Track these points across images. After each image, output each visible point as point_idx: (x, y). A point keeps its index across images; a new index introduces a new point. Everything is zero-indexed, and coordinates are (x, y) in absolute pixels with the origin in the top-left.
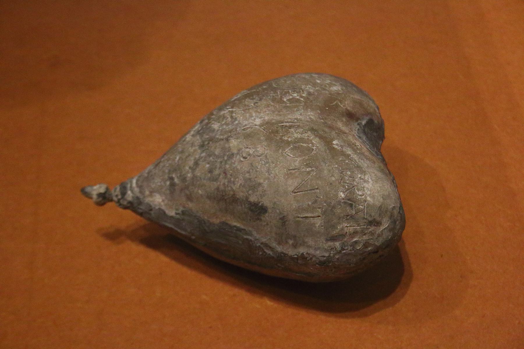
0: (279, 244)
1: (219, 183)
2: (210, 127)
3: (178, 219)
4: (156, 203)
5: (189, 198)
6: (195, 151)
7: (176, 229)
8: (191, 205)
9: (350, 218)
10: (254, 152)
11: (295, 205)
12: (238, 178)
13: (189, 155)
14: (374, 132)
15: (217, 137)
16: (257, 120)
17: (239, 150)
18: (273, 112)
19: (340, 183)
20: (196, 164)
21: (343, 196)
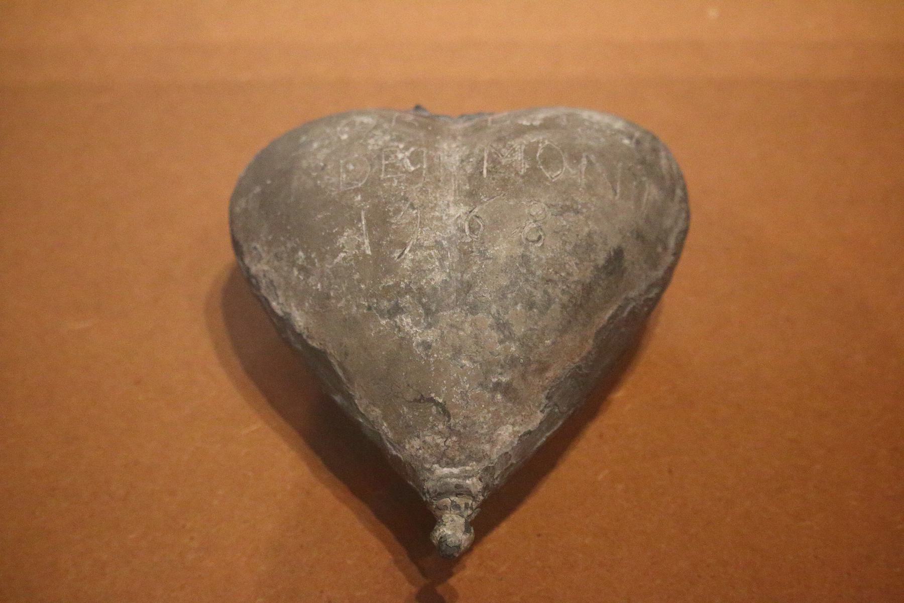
1: (557, 300)
5: (543, 368)
6: (473, 324)
8: (550, 374)
13: (476, 337)
20: (501, 326)
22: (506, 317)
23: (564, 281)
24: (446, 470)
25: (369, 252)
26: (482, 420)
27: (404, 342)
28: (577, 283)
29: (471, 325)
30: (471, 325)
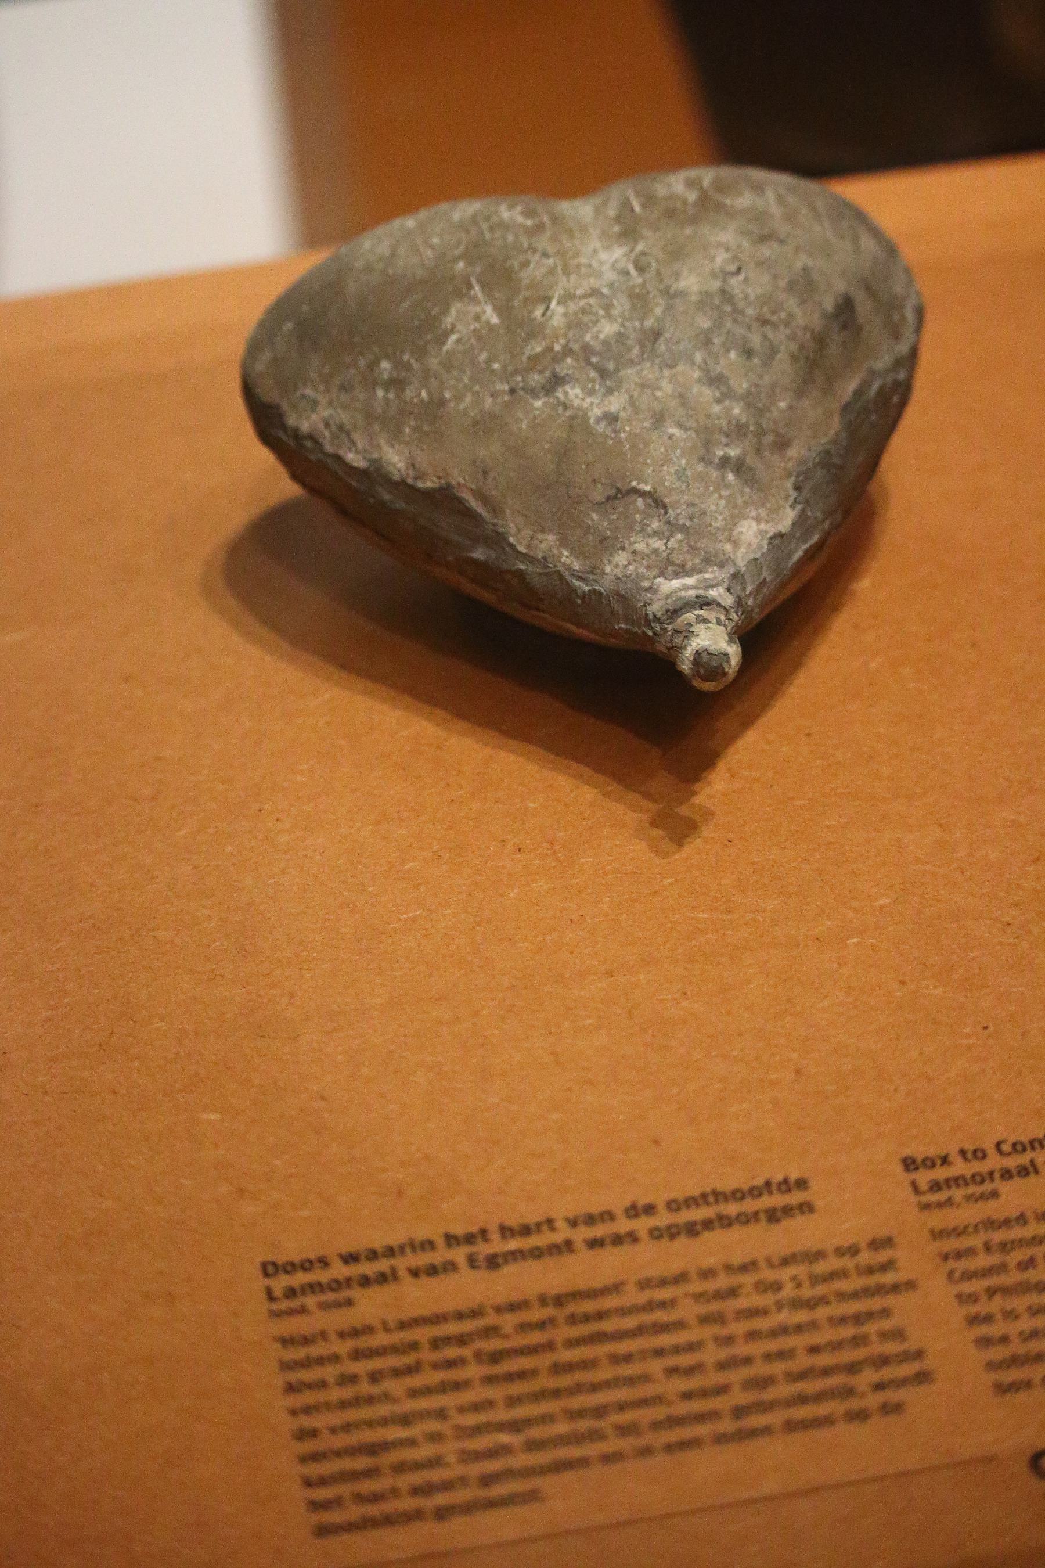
4: (755, 541)
5: (782, 445)
6: (673, 379)
8: (792, 452)
13: (681, 396)
20: (715, 380)
22: (718, 369)
24: (676, 583)
25: (495, 320)
26: (713, 508)
27: (577, 422)
28: (805, 328)
29: (670, 382)
30: (670, 382)
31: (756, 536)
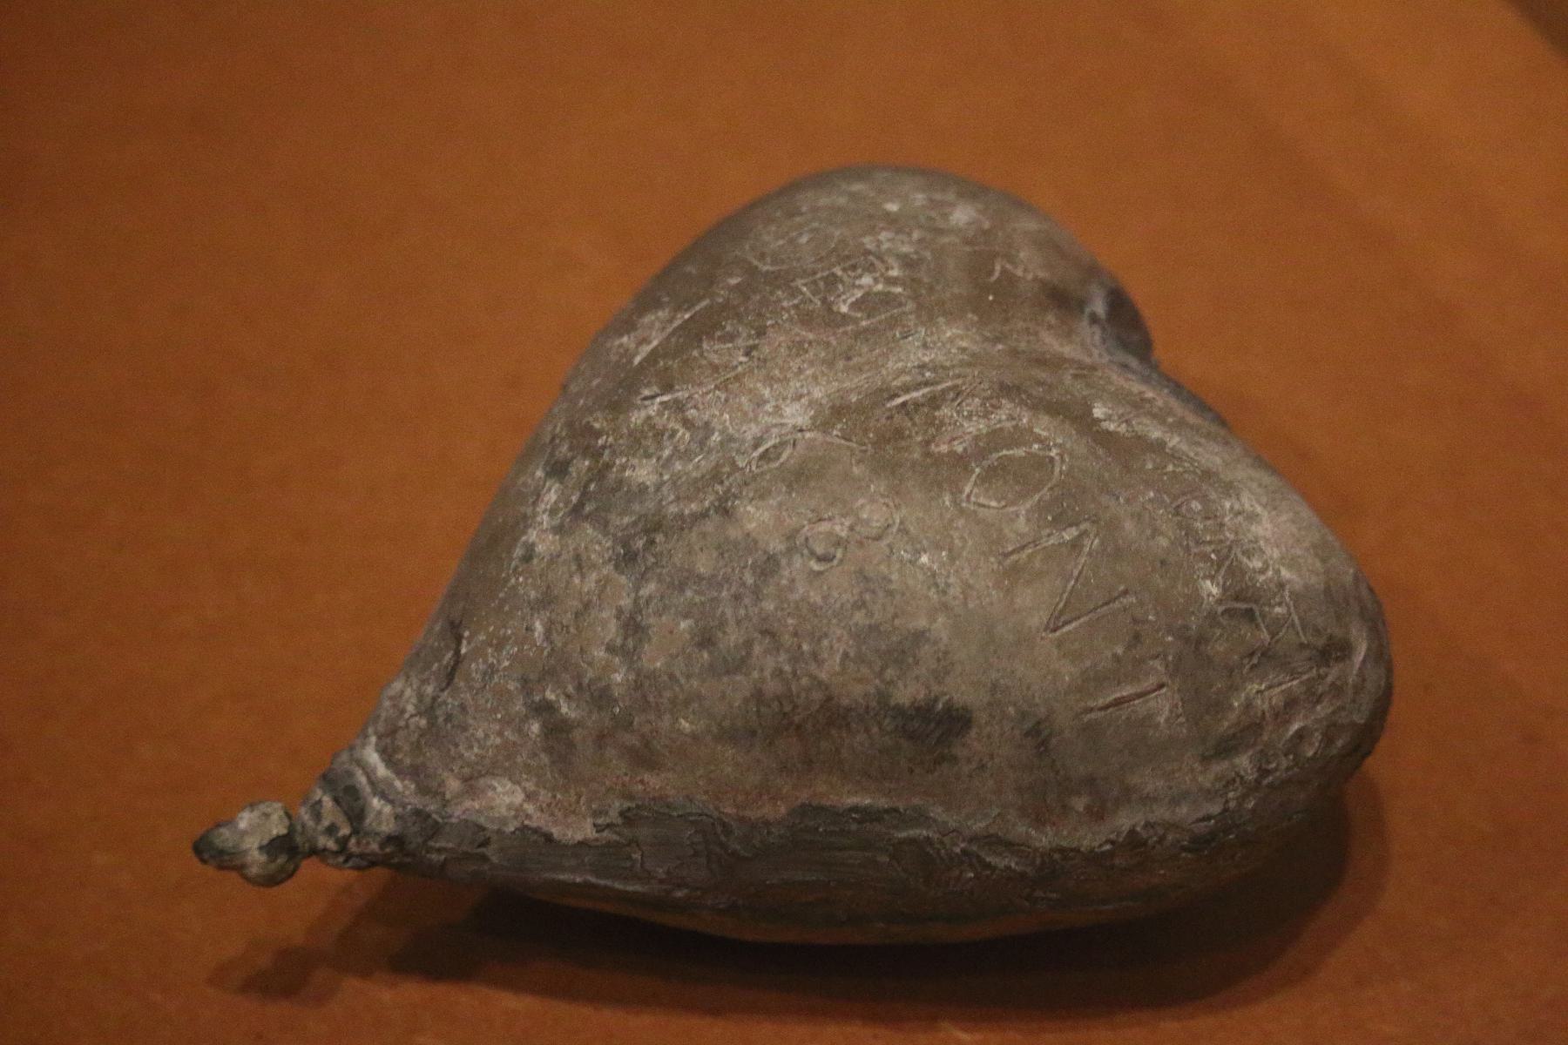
0: (1039, 821)
1: (755, 675)
2: (620, 482)
3: (609, 844)
5: (644, 758)
6: (604, 583)
7: (602, 882)
8: (654, 781)
9: (1265, 658)
10: (851, 528)
11: (1068, 672)
12: (826, 635)
13: (587, 606)
14: (1126, 324)
15: (673, 509)
16: (788, 411)
17: (791, 536)
18: (831, 364)
19: (1187, 549)
20: (633, 626)
21: (1215, 590)
22: (652, 621)
23: (796, 657)
25: (637, 360)
26: (480, 734)
31: (509, 807)
